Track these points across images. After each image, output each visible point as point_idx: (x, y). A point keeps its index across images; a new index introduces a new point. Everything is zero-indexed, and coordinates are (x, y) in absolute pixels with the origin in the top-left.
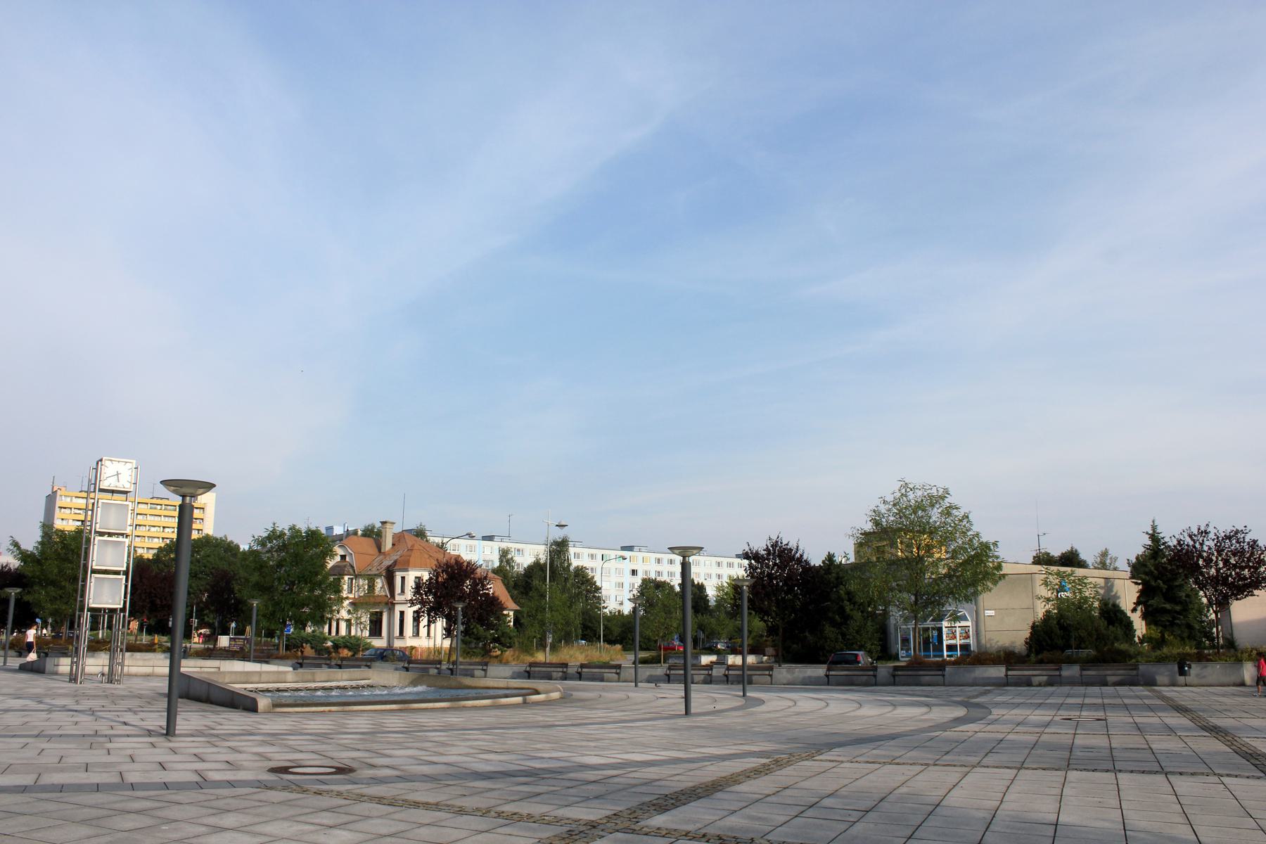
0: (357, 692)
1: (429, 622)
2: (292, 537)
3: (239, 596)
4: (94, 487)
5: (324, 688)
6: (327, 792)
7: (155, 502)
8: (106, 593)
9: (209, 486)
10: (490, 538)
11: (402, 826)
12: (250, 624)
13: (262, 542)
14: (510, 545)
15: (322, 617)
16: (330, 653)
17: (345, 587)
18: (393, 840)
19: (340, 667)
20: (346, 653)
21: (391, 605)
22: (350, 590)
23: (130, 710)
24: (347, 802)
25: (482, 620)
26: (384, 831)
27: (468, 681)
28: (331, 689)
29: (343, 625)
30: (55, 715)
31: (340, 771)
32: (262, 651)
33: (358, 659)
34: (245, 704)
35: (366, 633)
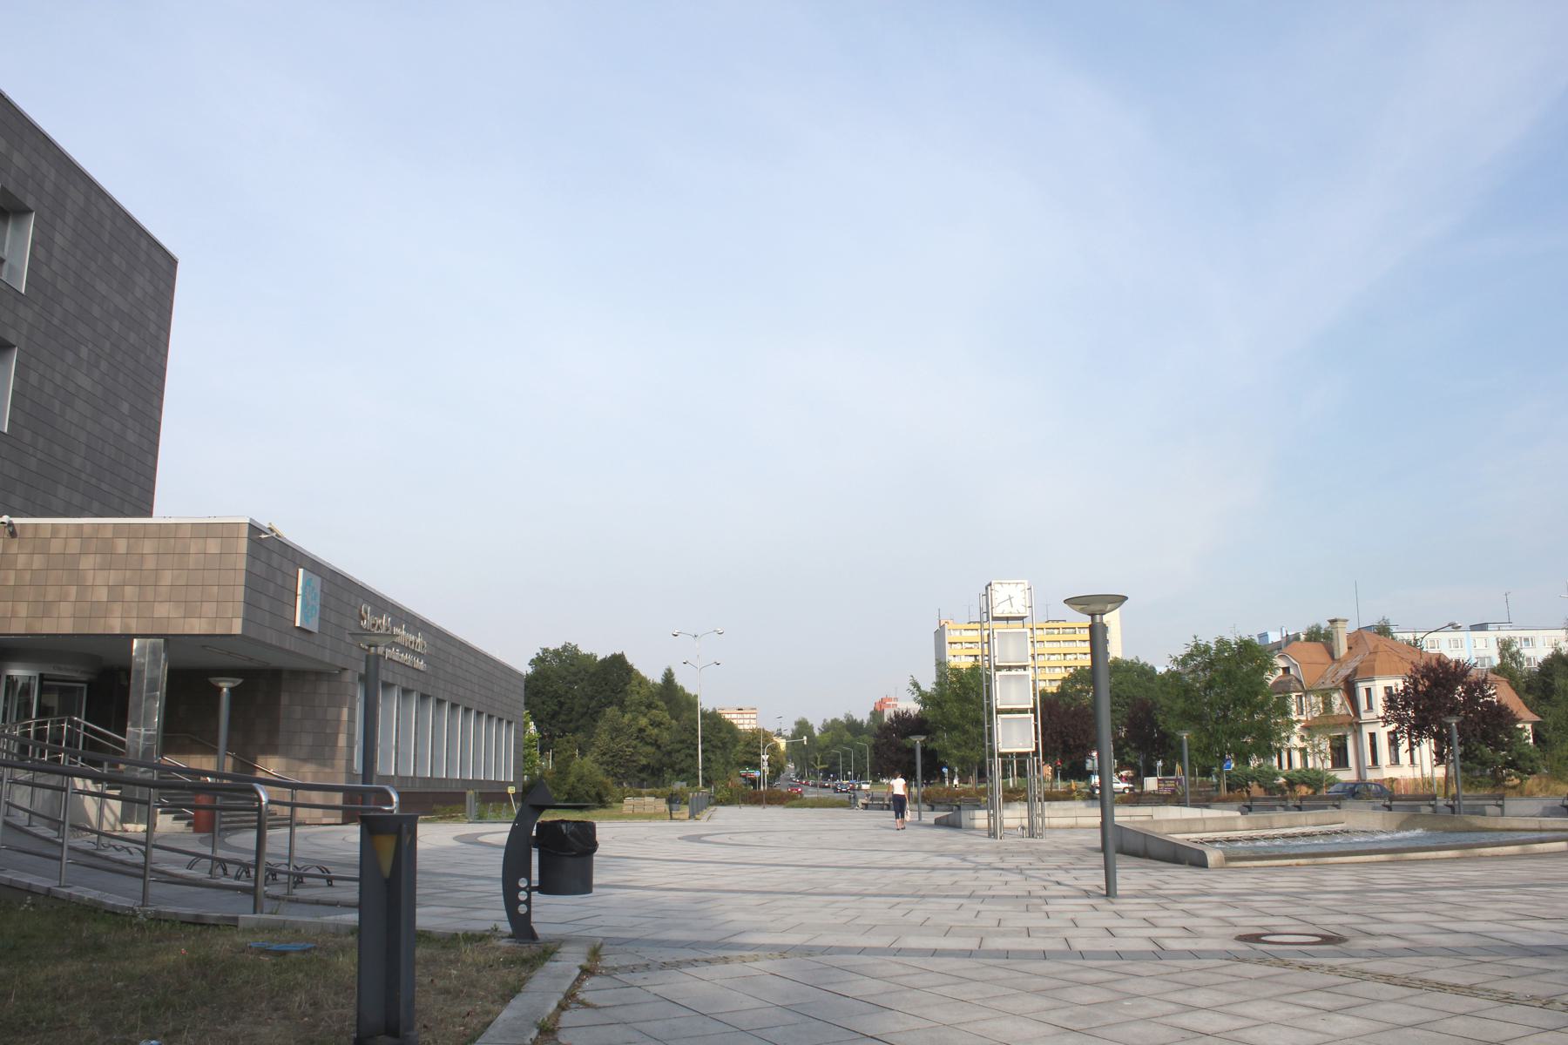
0: (1329, 840)
1: (1411, 744)
2: (1220, 651)
3: (1173, 730)
4: (988, 615)
5: (1285, 836)
6: (1317, 966)
7: (1052, 625)
8: (1016, 735)
9: (1120, 600)
10: (1482, 627)
11: (1426, 1015)
12: (1181, 761)
13: (1184, 662)
14: (1512, 634)
15: (1270, 747)
16: (1283, 792)
17: (1294, 708)
18: (1417, 1032)
19: (1300, 808)
20: (1304, 790)
21: (1356, 726)
22: (1303, 710)
23: (1059, 868)
24: (1345, 980)
25: (1485, 738)
26: (1402, 1020)
27: (1478, 821)
28: (1294, 836)
29: (1296, 756)
30: (982, 874)
31: (1327, 940)
32: (1199, 793)
33: (1321, 798)
34: (1191, 858)
35: (1329, 764)
